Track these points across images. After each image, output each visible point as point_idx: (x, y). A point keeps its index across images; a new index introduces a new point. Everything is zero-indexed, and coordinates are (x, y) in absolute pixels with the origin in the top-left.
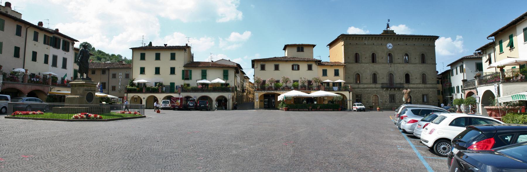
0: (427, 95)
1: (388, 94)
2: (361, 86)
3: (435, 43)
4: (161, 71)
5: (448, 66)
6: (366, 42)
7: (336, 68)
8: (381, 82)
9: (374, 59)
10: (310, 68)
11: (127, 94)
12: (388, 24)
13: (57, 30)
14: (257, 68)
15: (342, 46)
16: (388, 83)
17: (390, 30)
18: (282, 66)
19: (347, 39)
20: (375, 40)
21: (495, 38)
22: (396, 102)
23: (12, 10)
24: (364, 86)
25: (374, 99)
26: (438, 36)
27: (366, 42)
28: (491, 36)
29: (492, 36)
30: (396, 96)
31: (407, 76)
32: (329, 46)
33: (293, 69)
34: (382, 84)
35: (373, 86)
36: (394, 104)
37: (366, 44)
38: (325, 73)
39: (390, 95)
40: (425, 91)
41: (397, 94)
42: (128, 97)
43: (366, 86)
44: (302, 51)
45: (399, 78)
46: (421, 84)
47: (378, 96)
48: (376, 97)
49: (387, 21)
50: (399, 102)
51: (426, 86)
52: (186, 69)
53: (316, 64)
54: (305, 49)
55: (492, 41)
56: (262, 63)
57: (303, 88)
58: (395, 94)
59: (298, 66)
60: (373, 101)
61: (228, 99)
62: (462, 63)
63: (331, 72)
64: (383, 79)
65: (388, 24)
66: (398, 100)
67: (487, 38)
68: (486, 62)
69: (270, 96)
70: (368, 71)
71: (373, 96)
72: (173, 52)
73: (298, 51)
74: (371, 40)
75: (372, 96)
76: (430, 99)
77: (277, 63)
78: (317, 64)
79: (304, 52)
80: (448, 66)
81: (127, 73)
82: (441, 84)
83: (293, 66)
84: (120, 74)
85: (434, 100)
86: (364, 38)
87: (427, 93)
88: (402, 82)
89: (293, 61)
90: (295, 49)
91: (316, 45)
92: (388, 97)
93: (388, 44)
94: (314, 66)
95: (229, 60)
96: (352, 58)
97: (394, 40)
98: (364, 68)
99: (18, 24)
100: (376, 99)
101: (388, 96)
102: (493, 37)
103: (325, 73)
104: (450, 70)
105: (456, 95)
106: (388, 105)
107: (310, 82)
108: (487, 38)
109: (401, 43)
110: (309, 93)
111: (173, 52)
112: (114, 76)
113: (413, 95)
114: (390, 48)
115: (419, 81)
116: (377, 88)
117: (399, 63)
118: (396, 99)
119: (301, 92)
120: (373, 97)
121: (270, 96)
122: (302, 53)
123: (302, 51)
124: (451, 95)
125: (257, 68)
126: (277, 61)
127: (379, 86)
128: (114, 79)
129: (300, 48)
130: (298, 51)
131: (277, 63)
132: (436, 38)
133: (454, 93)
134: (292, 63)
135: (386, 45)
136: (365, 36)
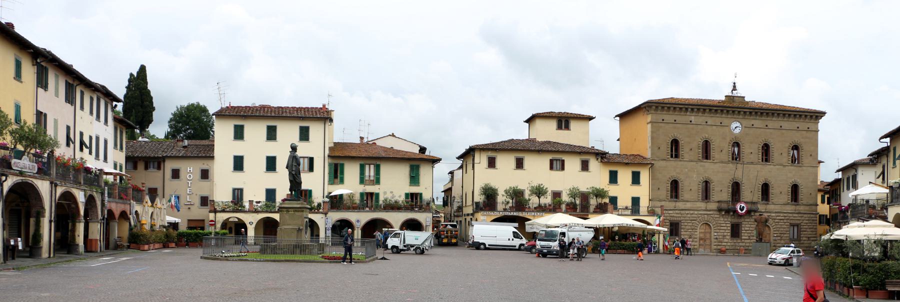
0: (797, 225)
1: (729, 222)
2: (680, 205)
4: (263, 164)
5: (838, 171)
8: (717, 199)
9: (706, 150)
10: (585, 166)
11: (215, 214)
13: (126, 87)
15: (648, 123)
16: (730, 201)
17: (739, 95)
18: (530, 161)
22: (743, 237)
24: (686, 204)
25: (703, 231)
27: (693, 118)
28: (885, 136)
29: (886, 138)
30: (743, 226)
31: (765, 189)
32: (618, 118)
33: (551, 168)
34: (718, 202)
35: (702, 205)
36: (739, 241)
37: (693, 121)
38: (613, 178)
39: (732, 224)
40: (796, 219)
42: (217, 219)
43: (688, 205)
44: (567, 127)
45: (750, 191)
46: (788, 204)
47: (711, 225)
48: (707, 227)
50: (747, 238)
51: (798, 207)
52: (43, 114)
53: (597, 160)
54: (573, 124)
55: (885, 145)
56: (491, 154)
59: (563, 161)
60: (702, 235)
61: (424, 225)
62: (855, 170)
63: (625, 175)
64: (721, 193)
65: (734, 83)
66: (746, 234)
70: (695, 176)
71: (700, 226)
72: (305, 124)
73: (560, 127)
75: (700, 225)
77: (520, 155)
78: (599, 159)
79: (570, 130)
80: (838, 171)
81: (205, 167)
82: (829, 203)
83: (551, 161)
84: (189, 169)
85: (810, 236)
87: (797, 222)
88: (755, 200)
90: (553, 124)
91: (595, 118)
92: (729, 228)
93: (733, 124)
94: (594, 164)
95: (393, 134)
96: (666, 148)
98: (686, 170)
100: (706, 231)
101: (729, 225)
102: (888, 140)
103: (613, 178)
104: (841, 179)
106: (729, 244)
107: (585, 197)
108: (880, 140)
109: (758, 122)
110: (585, 219)
111: (305, 124)
112: (176, 174)
113: (774, 224)
114: (737, 131)
115: (786, 197)
116: (710, 210)
117: (752, 163)
118: (743, 232)
119: (570, 215)
120: (702, 227)
122: (566, 132)
123: (567, 127)
126: (521, 150)
127: (714, 206)
128: (176, 181)
129: (564, 121)
130: (560, 127)
132: (822, 115)
135: (728, 126)
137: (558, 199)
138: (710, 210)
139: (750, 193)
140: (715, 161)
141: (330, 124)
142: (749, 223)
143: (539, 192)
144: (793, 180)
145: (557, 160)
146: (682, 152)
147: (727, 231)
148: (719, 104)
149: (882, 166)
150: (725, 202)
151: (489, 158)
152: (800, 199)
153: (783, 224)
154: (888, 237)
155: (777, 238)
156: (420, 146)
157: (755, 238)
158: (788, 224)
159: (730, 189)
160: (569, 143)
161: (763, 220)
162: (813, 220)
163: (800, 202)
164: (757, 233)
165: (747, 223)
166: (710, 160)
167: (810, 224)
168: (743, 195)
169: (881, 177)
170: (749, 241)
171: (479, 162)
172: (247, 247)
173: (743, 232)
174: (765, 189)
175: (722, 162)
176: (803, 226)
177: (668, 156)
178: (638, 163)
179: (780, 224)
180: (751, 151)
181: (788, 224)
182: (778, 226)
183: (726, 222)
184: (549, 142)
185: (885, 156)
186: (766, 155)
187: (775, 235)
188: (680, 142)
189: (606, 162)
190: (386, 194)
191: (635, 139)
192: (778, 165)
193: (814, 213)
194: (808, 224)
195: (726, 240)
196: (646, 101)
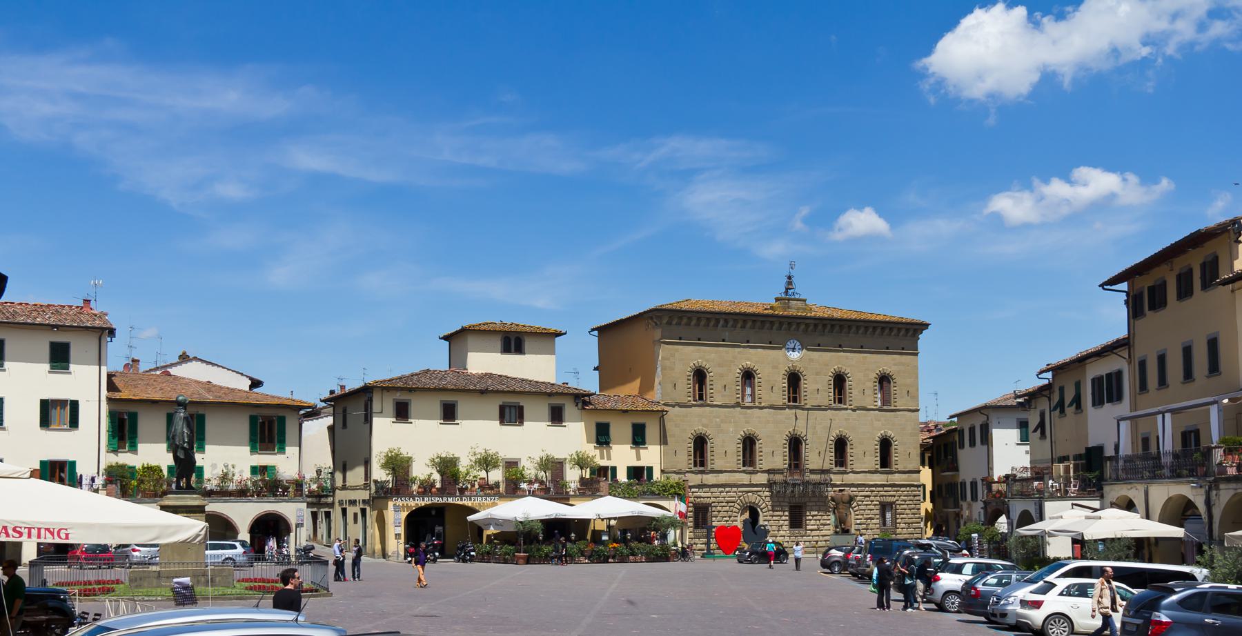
3: (919, 341)
6: (727, 334)
7: (639, 420)
12: (789, 278)
14: (382, 412)
19: (671, 324)
20: (754, 328)
21: (1053, 376)
22: (809, 527)
23: (303, 425)
26: (927, 322)
31: (841, 445)
39: (791, 507)
41: (810, 504)
43: (723, 478)
44: (519, 350)
45: (817, 451)
46: (875, 472)
49: (788, 266)
50: (816, 527)
53: (577, 405)
55: (1046, 382)
56: (400, 396)
57: (555, 490)
58: (805, 503)
64: (773, 456)
65: (789, 278)
66: (812, 522)
67: (1037, 375)
68: (1035, 431)
69: (433, 513)
70: (731, 430)
73: (506, 350)
74: (741, 327)
76: (902, 516)
86: (722, 322)
88: (827, 466)
89: (503, 392)
91: (565, 334)
97: (807, 330)
98: (718, 420)
99: (168, 412)
102: (1049, 375)
105: (970, 507)
108: (1037, 375)
115: (873, 461)
116: (756, 486)
118: (807, 518)
121: (433, 513)
124: (957, 505)
125: (382, 412)
131: (449, 398)
133: (966, 500)
134: (500, 400)
136: (724, 316)
137: (513, 470)
138: (756, 486)
139: (817, 456)
140: (763, 405)
141: (109, 339)
142: (818, 504)
143: (487, 462)
144: (882, 432)
145: (510, 407)
146: (712, 391)
147: (784, 518)
148: (767, 312)
149: (1038, 413)
150: (780, 472)
151: (444, 405)
152: (893, 463)
153: (870, 503)
154: (1227, 487)
155: (861, 527)
156: (251, 379)
157: (832, 527)
158: (878, 503)
159: (849, 450)
160: (525, 377)
161: (846, 498)
162: (915, 496)
163: (894, 468)
164: (836, 519)
165: (814, 504)
166: (845, 404)
167: (911, 502)
168: (806, 462)
169: (1039, 431)
170: (817, 533)
171: (380, 411)
172: (879, 499)
173: (807, 518)
174: (841, 445)
175: (771, 407)
176: (900, 505)
177: (689, 398)
178: (642, 411)
179: (865, 503)
180: (816, 387)
181: (878, 503)
182: (861, 507)
183: (782, 504)
184: (491, 376)
185: (1047, 399)
186: (840, 393)
187: (858, 522)
188: (802, 381)
189: (592, 409)
190: (216, 468)
191: (630, 369)
192: (858, 409)
193: (915, 483)
194: (908, 502)
195: (782, 533)
196: (652, 307)
